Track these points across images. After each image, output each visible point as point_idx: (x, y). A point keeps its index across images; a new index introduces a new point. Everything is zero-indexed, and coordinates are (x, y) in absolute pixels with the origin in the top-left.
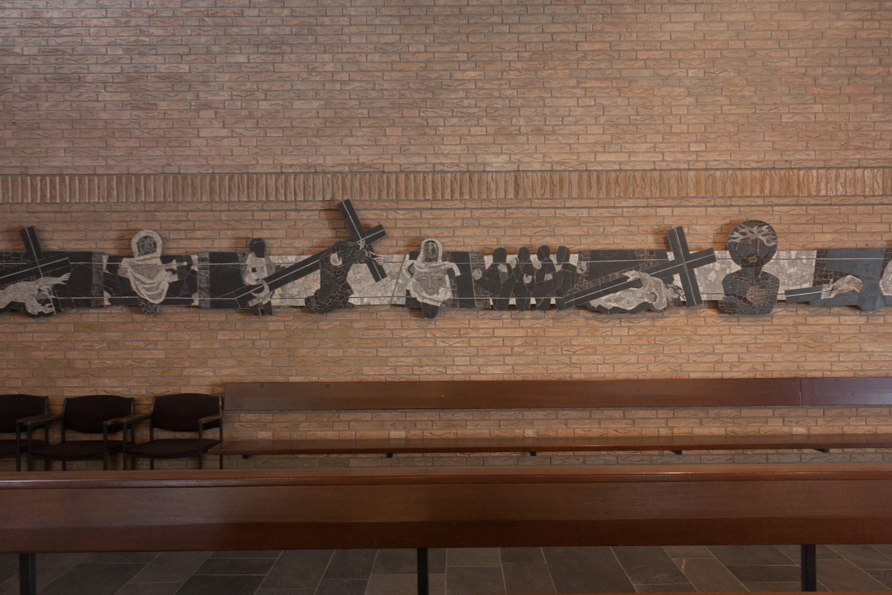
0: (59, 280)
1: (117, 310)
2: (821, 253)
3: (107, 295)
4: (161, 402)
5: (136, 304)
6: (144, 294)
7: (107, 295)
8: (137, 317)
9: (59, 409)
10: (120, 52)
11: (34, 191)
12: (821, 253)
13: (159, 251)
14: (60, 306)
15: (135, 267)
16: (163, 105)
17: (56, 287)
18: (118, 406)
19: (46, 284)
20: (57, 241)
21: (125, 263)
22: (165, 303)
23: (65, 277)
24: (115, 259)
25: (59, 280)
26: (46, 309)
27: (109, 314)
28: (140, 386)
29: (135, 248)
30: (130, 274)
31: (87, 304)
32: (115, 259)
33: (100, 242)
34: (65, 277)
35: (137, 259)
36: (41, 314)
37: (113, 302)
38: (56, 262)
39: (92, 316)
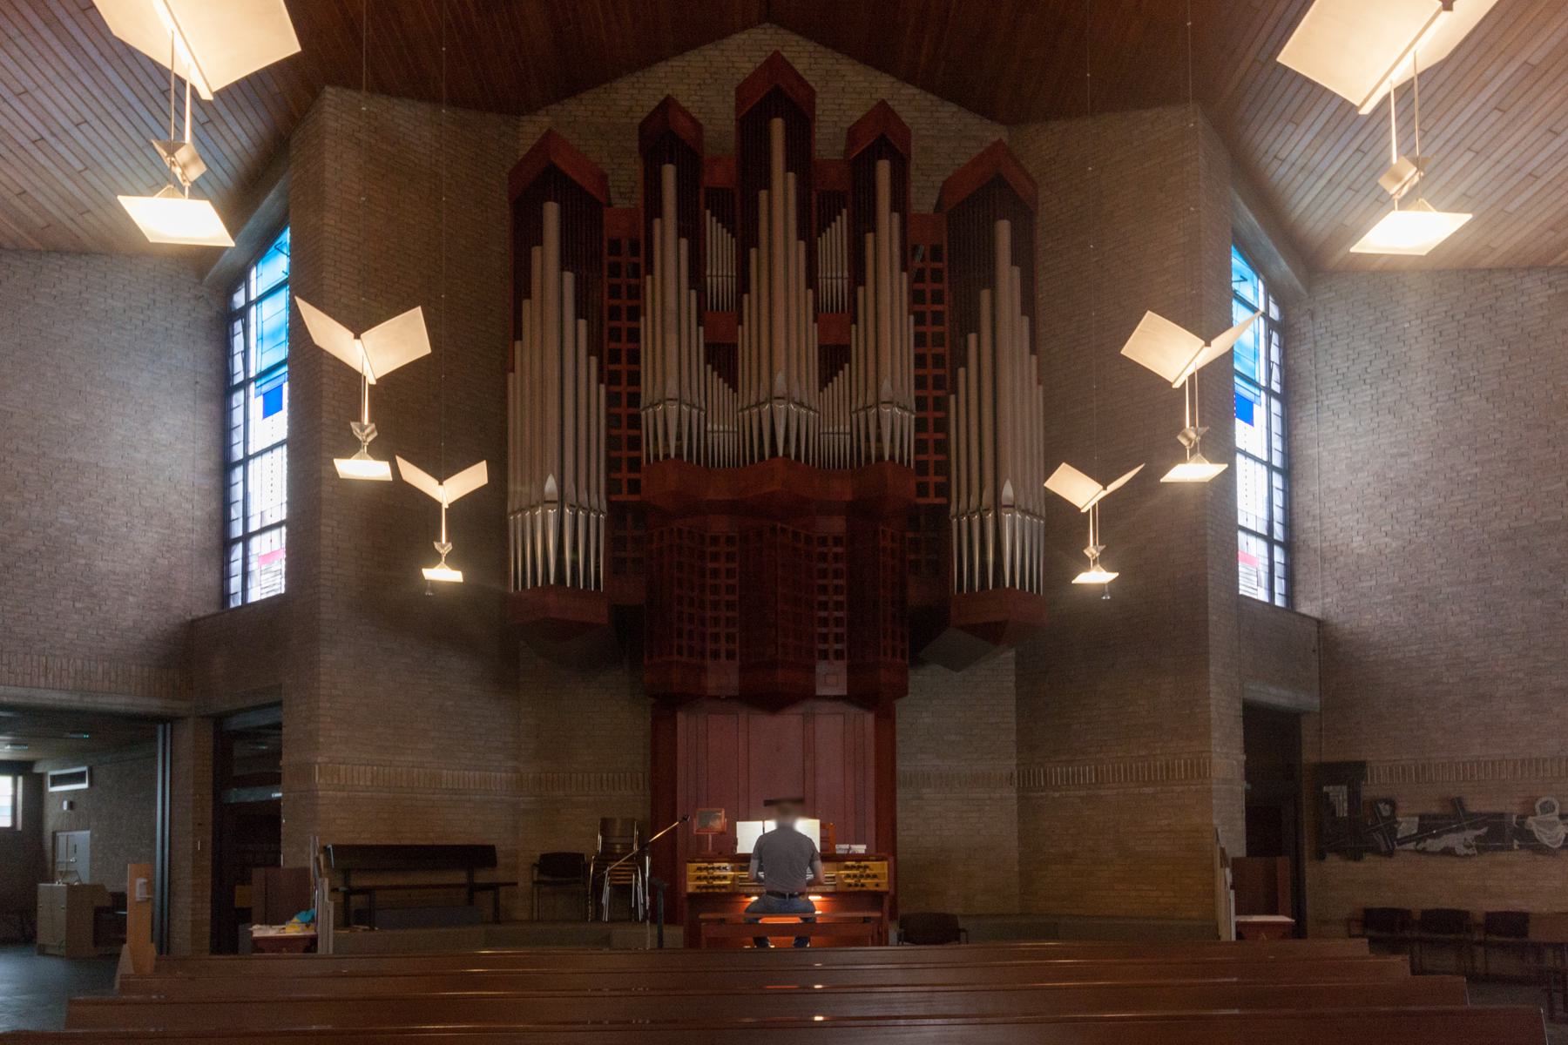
0: (1477, 833)
1: (1523, 853)
2: (1422, 817)
3: (1516, 842)
4: (1425, 913)
5: (1539, 849)
6: (1546, 841)
7: (1516, 842)
8: (1539, 857)
9: (1417, 917)
10: (1521, 675)
11: (1458, 773)
12: (1422, 817)
13: (1557, 811)
14: (1482, 850)
15: (1538, 823)
16: (1556, 709)
17: (1478, 838)
18: (1405, 913)
19: (1470, 835)
20: (1475, 805)
21: (1530, 820)
22: (1563, 847)
23: (1485, 830)
24: (1522, 817)
25: (1477, 833)
26: (1470, 852)
27: (1517, 856)
28: (1482, 906)
29: (1537, 806)
30: (1534, 828)
31: (1502, 849)
32: (1522, 817)
33: (1510, 806)
34: (1485, 830)
35: (1540, 817)
36: (1467, 855)
37: (1521, 847)
38: (1476, 820)
39: (1503, 856)
